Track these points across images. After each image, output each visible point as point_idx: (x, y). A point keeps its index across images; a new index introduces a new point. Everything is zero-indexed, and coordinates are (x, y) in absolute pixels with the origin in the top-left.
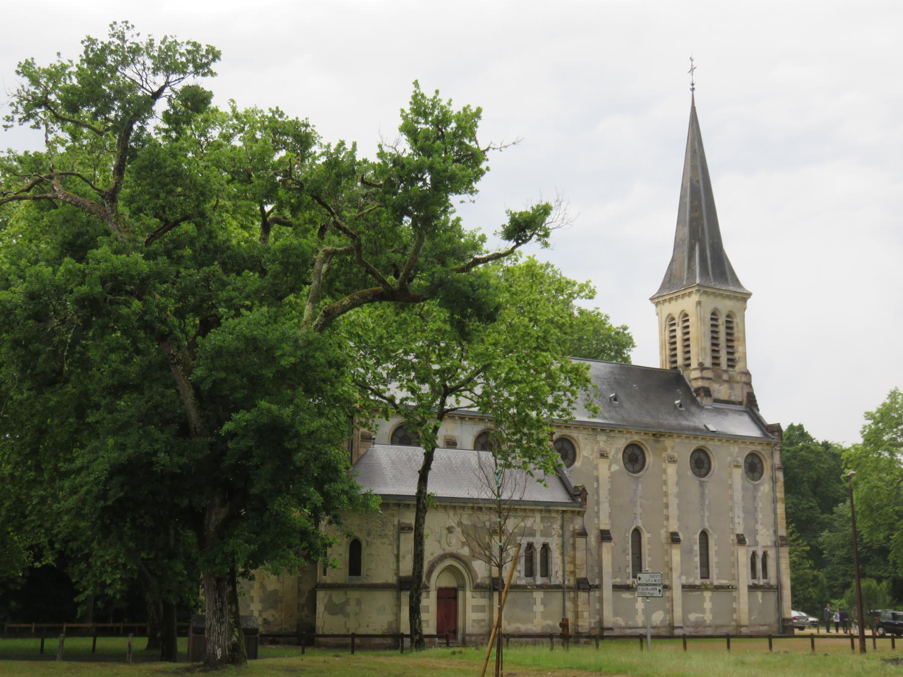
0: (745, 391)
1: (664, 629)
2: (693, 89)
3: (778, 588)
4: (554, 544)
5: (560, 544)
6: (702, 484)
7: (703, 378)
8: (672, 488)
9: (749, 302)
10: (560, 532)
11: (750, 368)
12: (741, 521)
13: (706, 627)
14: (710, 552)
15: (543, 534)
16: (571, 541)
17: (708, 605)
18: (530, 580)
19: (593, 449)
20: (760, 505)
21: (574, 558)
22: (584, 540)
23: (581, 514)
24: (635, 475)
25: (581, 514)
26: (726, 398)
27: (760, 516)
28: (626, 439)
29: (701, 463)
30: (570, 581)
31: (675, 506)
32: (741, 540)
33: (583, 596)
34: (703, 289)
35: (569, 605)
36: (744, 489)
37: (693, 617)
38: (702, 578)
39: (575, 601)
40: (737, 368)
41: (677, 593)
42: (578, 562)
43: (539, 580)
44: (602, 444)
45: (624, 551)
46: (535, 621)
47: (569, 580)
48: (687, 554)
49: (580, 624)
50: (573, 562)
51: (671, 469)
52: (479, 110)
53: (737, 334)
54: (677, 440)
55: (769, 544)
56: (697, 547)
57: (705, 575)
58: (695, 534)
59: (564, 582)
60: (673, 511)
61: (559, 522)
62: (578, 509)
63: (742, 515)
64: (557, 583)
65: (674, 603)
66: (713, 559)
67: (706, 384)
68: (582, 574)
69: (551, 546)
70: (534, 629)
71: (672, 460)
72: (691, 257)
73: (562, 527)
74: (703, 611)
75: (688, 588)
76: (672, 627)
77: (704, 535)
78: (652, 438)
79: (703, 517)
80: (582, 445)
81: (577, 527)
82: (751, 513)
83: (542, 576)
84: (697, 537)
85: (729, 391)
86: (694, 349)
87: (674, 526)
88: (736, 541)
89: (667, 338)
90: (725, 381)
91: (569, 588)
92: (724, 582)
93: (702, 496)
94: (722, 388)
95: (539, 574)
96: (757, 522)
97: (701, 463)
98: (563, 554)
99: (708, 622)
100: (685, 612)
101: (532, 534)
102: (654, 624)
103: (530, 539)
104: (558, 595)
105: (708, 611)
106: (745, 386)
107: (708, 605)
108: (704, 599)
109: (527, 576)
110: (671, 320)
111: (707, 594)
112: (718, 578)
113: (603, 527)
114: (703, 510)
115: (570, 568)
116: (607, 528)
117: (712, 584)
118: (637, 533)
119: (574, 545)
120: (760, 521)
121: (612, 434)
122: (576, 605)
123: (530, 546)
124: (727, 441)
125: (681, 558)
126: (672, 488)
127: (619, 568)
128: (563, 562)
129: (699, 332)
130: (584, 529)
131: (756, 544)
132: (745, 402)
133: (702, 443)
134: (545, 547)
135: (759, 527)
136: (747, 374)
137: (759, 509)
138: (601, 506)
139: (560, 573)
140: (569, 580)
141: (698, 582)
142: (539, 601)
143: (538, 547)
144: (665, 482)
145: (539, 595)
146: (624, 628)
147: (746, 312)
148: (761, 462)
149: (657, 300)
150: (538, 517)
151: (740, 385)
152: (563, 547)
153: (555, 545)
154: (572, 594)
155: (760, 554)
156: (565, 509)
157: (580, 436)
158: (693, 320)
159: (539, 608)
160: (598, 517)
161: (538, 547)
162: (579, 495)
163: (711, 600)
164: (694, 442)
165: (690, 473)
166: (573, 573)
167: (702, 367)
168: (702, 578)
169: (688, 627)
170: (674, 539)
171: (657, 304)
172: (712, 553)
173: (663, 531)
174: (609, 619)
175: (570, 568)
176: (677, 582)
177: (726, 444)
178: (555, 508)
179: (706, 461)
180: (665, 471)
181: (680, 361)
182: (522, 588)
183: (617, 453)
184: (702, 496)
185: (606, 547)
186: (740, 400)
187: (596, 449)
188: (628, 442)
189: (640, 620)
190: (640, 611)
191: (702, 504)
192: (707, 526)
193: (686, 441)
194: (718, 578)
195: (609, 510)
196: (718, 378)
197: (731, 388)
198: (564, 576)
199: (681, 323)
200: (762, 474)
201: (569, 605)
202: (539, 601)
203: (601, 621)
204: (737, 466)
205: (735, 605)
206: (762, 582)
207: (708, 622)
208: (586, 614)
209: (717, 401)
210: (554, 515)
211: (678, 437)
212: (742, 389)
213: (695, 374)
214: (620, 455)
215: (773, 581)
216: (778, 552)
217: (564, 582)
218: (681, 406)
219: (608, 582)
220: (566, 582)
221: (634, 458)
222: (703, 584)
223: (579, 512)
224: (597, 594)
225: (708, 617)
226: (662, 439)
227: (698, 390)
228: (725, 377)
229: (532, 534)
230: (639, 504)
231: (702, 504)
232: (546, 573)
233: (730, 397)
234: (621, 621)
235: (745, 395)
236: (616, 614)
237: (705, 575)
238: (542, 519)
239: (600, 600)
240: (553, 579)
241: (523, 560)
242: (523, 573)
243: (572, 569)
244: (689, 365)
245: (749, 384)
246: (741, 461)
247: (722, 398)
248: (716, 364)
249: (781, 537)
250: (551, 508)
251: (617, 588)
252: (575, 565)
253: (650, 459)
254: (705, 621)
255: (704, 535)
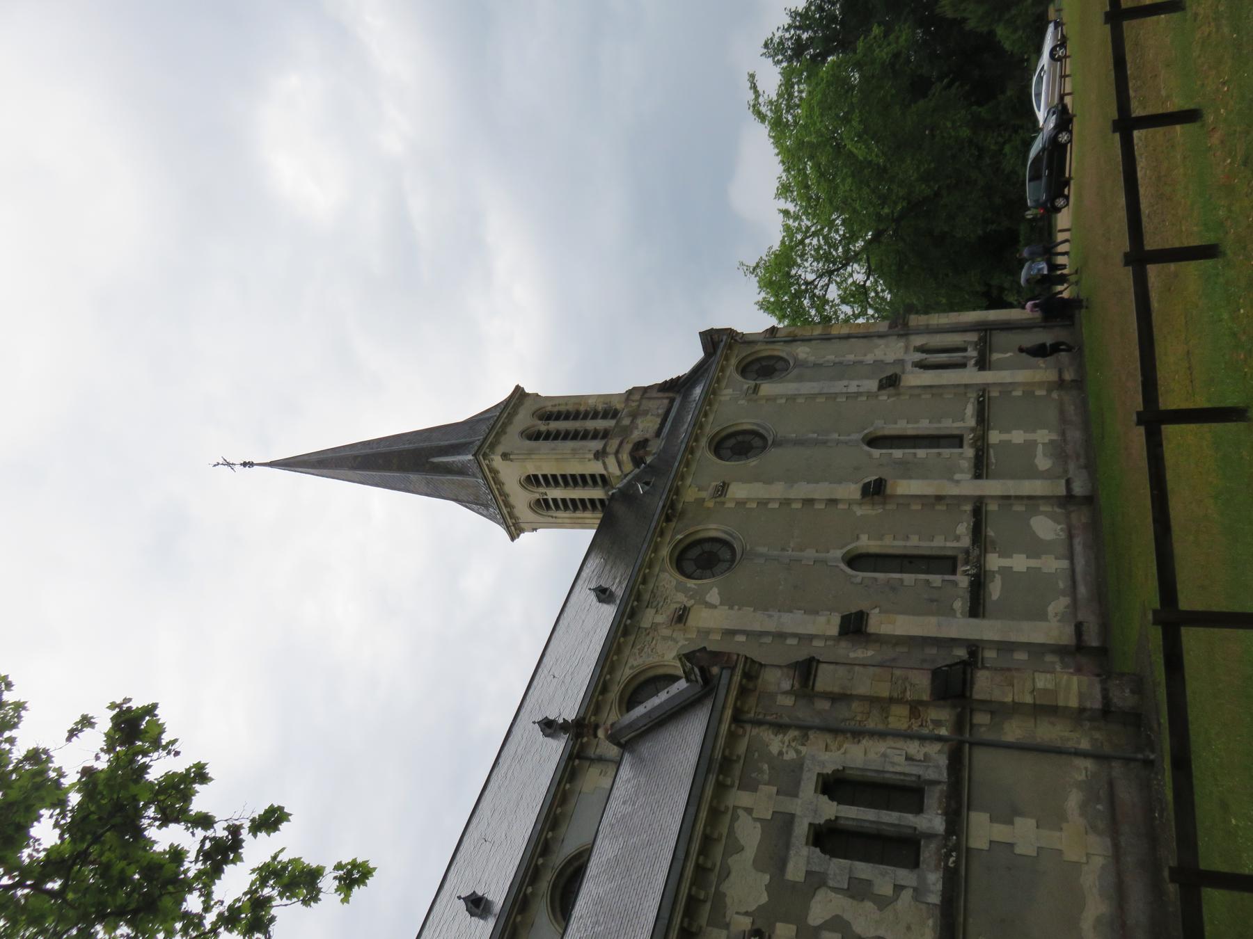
0: (655, 394)
1: (1074, 516)
2: (251, 464)
3: (985, 329)
4: (825, 756)
5: (828, 738)
6: (778, 443)
7: (617, 453)
8: (777, 490)
9: (527, 390)
10: (793, 733)
11: (622, 390)
12: (855, 383)
13: (1065, 441)
14: (910, 432)
15: (791, 790)
16: (824, 705)
17: (1018, 437)
18: (929, 852)
19: (665, 638)
20: (832, 357)
21: (873, 700)
22: (822, 667)
23: (752, 670)
24: (738, 557)
25: (752, 670)
26: (659, 420)
27: (851, 357)
28: (662, 570)
29: (740, 445)
30: (941, 718)
31: (812, 486)
32: (891, 382)
33: (984, 685)
34: (485, 448)
35: (1014, 731)
36: (800, 379)
37: (1043, 462)
38: (961, 446)
39: (1002, 711)
40: (619, 406)
41: (991, 487)
42: (884, 691)
43: (932, 821)
44: (660, 619)
45: (893, 589)
46: (1072, 855)
47: (938, 723)
48: (906, 470)
49: (1074, 703)
50: (882, 704)
51: (738, 491)
52: (211, 779)
53: (570, 408)
54: (689, 481)
55: (901, 344)
56: (898, 453)
57: (956, 440)
58: (870, 456)
59: (939, 739)
60: (820, 491)
61: (766, 735)
62: (737, 678)
63: (845, 383)
64: (943, 761)
65: (1012, 493)
66: (924, 426)
67: (628, 447)
68: (921, 683)
69: (828, 770)
70: (1098, 862)
71: (723, 489)
72: (447, 470)
73: (780, 728)
74: (1030, 446)
75: (980, 469)
76: (1068, 500)
77: (875, 441)
78: (673, 524)
79: (838, 442)
80: (653, 660)
81: (786, 685)
82: (842, 370)
83: (919, 809)
84: (876, 453)
85: (649, 417)
86: (575, 468)
87: (852, 491)
88: (891, 390)
89: (567, 514)
90: (632, 422)
91: (960, 724)
92: (970, 410)
93: (799, 443)
94: (641, 426)
95: (911, 819)
96: (861, 362)
97: (740, 445)
98: (858, 734)
99: (1054, 437)
100: (1032, 473)
101: (785, 822)
102: (1063, 535)
103: (801, 829)
104: (983, 762)
105: (1030, 436)
106: (647, 395)
107: (1018, 437)
108: (1006, 444)
109: (914, 863)
110: (543, 505)
111: (995, 437)
112: (963, 420)
113: (834, 630)
114: (825, 443)
115: (899, 718)
116: (836, 620)
117: (973, 430)
118: (856, 561)
119: (836, 698)
120: (859, 358)
121: (646, 597)
122: (1016, 709)
123: (827, 838)
124: (710, 404)
125: (917, 478)
126: (777, 490)
127: (932, 601)
128: (882, 735)
129: (547, 461)
130: (796, 666)
131: (901, 362)
132: (671, 395)
133: (704, 442)
134: (835, 786)
135: (869, 358)
136: (630, 392)
137: (837, 360)
138: (789, 629)
139: (914, 748)
140: (938, 723)
141: (969, 452)
142: (1000, 832)
143: (829, 810)
144: (763, 503)
145: (982, 830)
146: (1075, 600)
147: (542, 394)
148: (759, 360)
149: (514, 531)
150: (742, 798)
151: (644, 402)
152: (835, 731)
153: (827, 756)
154: (981, 718)
155: (918, 356)
156: (729, 713)
157: (632, 662)
158: (531, 469)
159: (1025, 835)
160: (811, 637)
161: (829, 810)
162: (702, 670)
163: (1008, 431)
164: (698, 454)
165: (753, 462)
166: (915, 708)
167: (600, 455)
168: (961, 446)
169: (1066, 471)
170: (875, 490)
171: (522, 531)
172: (910, 429)
173: (859, 511)
174: (1051, 629)
175: (899, 718)
176: (967, 486)
177: (715, 407)
178: (721, 742)
179: (740, 438)
180: (741, 503)
181: (597, 494)
182: (953, 882)
183: (685, 590)
184: (799, 443)
185: (878, 624)
186: (666, 402)
187: (666, 632)
188: (668, 565)
189: (1053, 564)
190: (1033, 563)
191: (816, 443)
192: (857, 436)
193: (693, 467)
194: (963, 420)
195: (799, 615)
196: (625, 432)
197: (646, 413)
198: (922, 739)
199: (541, 490)
200: (781, 358)
201: (1014, 731)
202: (1000, 832)
203: (1060, 651)
204: (756, 389)
205: (1018, 393)
206: (972, 353)
207: (1054, 437)
208: (1043, 681)
209: (658, 433)
210: (742, 747)
211: (683, 478)
212: (650, 398)
213: (613, 469)
214: (691, 584)
215: (973, 337)
216: (919, 331)
217: (939, 739)
218: (647, 483)
219: (961, 627)
220: (943, 732)
221: (703, 558)
222: (974, 445)
223: (747, 675)
224: (993, 507)
225: (1043, 436)
226: (680, 506)
227: (637, 461)
228: (626, 422)
229: (785, 822)
230: (797, 554)
231: (816, 443)
232: (907, 794)
233: (658, 415)
234: (1059, 605)
235: (661, 395)
236: (1043, 616)
237: (956, 440)
238: (749, 785)
239: (1006, 647)
240: (931, 775)
241: (863, 870)
242: (905, 876)
243: (903, 711)
244: (602, 476)
245: (645, 390)
246: (748, 384)
247: (657, 426)
248: (605, 435)
249: (890, 327)
250: (718, 755)
251: (976, 608)
252: (891, 700)
253: (713, 529)
254: (1052, 442)
255: (875, 441)
